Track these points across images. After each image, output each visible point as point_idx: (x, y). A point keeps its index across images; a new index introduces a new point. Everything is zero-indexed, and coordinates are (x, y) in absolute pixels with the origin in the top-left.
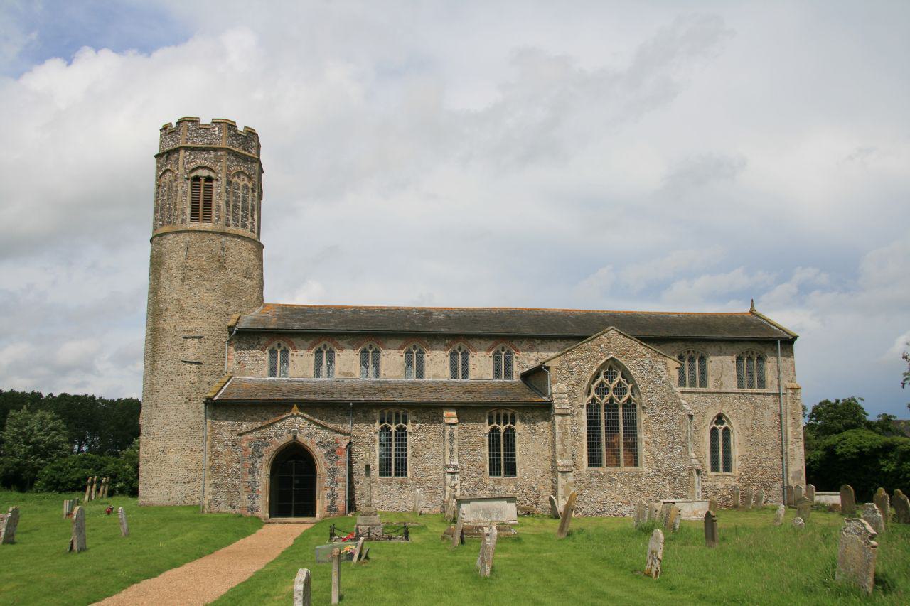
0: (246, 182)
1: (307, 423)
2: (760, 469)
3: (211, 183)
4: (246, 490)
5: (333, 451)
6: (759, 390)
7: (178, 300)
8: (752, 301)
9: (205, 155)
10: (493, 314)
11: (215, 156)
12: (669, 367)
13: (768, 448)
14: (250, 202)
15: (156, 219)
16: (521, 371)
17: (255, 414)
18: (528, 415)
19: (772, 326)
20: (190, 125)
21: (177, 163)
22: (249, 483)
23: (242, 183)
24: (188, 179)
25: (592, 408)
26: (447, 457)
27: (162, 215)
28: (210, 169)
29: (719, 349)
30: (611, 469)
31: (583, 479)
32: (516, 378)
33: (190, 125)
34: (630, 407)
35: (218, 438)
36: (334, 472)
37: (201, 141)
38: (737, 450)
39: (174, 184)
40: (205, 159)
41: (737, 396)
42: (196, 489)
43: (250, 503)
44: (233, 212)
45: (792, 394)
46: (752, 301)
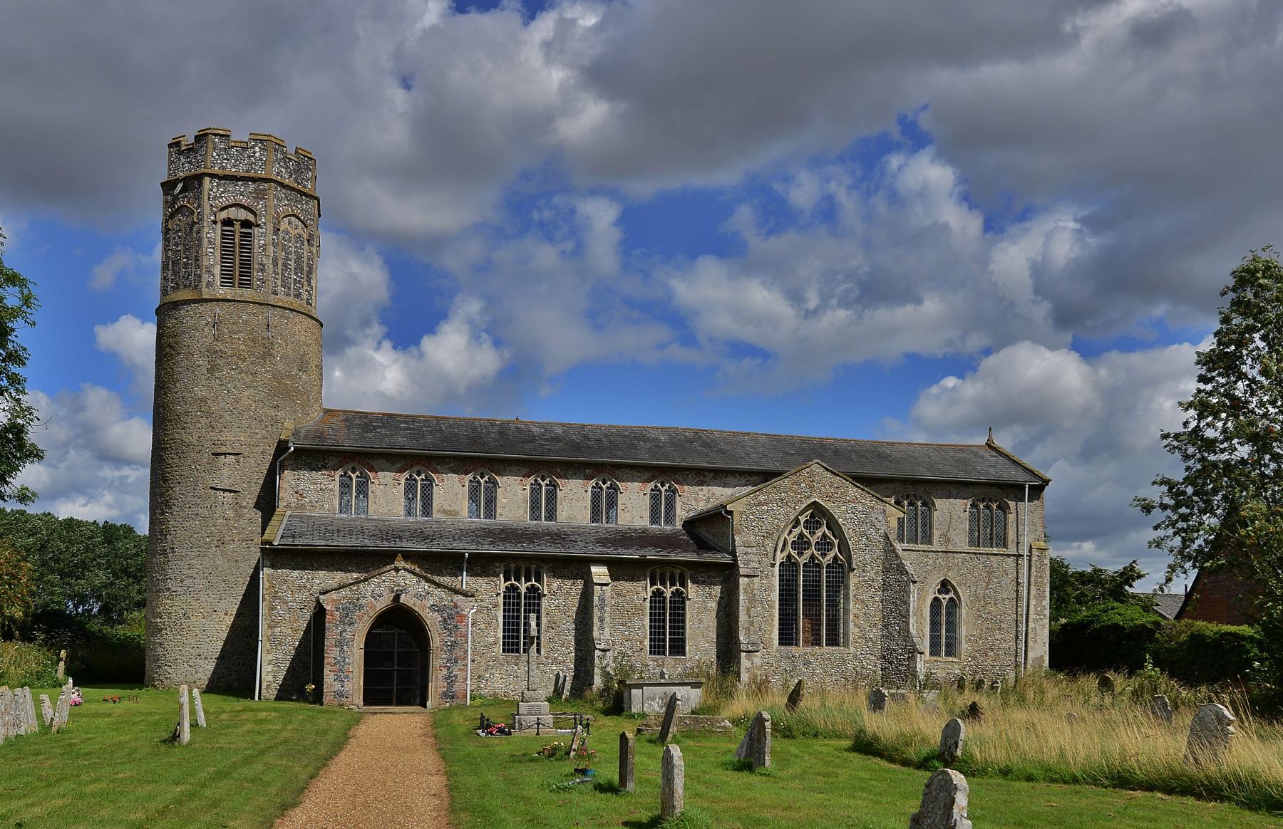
1: (415, 579)
5: (451, 617)
9: (240, 187)
11: (255, 190)
12: (890, 515)
13: (1003, 626)
14: (306, 261)
15: (165, 279)
18: (702, 575)
20: (216, 140)
23: (294, 232)
24: (215, 222)
25: (789, 567)
27: (175, 273)
30: (809, 649)
31: (770, 661)
32: (679, 525)
33: (216, 140)
35: (280, 598)
41: (967, 557)
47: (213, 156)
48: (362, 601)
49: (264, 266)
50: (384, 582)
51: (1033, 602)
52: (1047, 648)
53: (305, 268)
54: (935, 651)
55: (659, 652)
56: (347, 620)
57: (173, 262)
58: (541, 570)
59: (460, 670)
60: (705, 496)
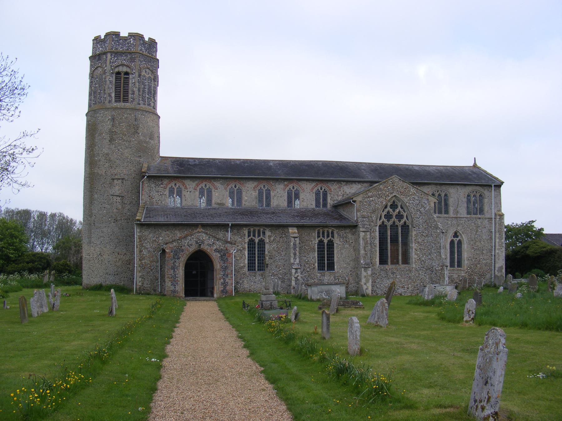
0: (150, 75)
2: (478, 266)
3: (128, 76)
4: (170, 280)
6: (480, 216)
7: (107, 154)
8: (475, 158)
10: (312, 165)
13: (484, 252)
14: (152, 88)
16: (332, 203)
17: (168, 230)
18: (342, 232)
19: (487, 175)
20: (114, 37)
21: (106, 63)
22: (171, 275)
23: (147, 76)
24: (113, 73)
25: (383, 227)
26: (292, 259)
27: (95, 97)
28: (127, 66)
29: (457, 190)
30: (394, 266)
31: (376, 272)
34: (405, 227)
35: (144, 246)
36: (225, 268)
37: (122, 48)
38: (466, 253)
39: (104, 77)
40: (124, 60)
42: (122, 279)
43: (172, 288)
44: (142, 95)
45: (499, 218)
46: (475, 158)
47: (112, 44)
48: (183, 248)
49: (134, 92)
50: (193, 238)
51: (497, 240)
52: (504, 262)
53: (152, 92)
54: (452, 265)
55: (322, 269)
56: (176, 255)
57: (94, 92)
58: (265, 231)
59: (229, 279)
60: (341, 193)
